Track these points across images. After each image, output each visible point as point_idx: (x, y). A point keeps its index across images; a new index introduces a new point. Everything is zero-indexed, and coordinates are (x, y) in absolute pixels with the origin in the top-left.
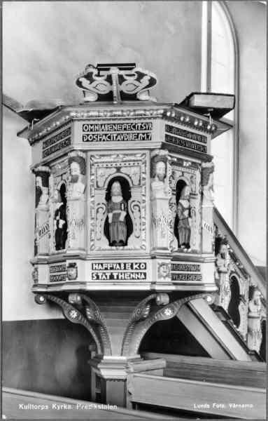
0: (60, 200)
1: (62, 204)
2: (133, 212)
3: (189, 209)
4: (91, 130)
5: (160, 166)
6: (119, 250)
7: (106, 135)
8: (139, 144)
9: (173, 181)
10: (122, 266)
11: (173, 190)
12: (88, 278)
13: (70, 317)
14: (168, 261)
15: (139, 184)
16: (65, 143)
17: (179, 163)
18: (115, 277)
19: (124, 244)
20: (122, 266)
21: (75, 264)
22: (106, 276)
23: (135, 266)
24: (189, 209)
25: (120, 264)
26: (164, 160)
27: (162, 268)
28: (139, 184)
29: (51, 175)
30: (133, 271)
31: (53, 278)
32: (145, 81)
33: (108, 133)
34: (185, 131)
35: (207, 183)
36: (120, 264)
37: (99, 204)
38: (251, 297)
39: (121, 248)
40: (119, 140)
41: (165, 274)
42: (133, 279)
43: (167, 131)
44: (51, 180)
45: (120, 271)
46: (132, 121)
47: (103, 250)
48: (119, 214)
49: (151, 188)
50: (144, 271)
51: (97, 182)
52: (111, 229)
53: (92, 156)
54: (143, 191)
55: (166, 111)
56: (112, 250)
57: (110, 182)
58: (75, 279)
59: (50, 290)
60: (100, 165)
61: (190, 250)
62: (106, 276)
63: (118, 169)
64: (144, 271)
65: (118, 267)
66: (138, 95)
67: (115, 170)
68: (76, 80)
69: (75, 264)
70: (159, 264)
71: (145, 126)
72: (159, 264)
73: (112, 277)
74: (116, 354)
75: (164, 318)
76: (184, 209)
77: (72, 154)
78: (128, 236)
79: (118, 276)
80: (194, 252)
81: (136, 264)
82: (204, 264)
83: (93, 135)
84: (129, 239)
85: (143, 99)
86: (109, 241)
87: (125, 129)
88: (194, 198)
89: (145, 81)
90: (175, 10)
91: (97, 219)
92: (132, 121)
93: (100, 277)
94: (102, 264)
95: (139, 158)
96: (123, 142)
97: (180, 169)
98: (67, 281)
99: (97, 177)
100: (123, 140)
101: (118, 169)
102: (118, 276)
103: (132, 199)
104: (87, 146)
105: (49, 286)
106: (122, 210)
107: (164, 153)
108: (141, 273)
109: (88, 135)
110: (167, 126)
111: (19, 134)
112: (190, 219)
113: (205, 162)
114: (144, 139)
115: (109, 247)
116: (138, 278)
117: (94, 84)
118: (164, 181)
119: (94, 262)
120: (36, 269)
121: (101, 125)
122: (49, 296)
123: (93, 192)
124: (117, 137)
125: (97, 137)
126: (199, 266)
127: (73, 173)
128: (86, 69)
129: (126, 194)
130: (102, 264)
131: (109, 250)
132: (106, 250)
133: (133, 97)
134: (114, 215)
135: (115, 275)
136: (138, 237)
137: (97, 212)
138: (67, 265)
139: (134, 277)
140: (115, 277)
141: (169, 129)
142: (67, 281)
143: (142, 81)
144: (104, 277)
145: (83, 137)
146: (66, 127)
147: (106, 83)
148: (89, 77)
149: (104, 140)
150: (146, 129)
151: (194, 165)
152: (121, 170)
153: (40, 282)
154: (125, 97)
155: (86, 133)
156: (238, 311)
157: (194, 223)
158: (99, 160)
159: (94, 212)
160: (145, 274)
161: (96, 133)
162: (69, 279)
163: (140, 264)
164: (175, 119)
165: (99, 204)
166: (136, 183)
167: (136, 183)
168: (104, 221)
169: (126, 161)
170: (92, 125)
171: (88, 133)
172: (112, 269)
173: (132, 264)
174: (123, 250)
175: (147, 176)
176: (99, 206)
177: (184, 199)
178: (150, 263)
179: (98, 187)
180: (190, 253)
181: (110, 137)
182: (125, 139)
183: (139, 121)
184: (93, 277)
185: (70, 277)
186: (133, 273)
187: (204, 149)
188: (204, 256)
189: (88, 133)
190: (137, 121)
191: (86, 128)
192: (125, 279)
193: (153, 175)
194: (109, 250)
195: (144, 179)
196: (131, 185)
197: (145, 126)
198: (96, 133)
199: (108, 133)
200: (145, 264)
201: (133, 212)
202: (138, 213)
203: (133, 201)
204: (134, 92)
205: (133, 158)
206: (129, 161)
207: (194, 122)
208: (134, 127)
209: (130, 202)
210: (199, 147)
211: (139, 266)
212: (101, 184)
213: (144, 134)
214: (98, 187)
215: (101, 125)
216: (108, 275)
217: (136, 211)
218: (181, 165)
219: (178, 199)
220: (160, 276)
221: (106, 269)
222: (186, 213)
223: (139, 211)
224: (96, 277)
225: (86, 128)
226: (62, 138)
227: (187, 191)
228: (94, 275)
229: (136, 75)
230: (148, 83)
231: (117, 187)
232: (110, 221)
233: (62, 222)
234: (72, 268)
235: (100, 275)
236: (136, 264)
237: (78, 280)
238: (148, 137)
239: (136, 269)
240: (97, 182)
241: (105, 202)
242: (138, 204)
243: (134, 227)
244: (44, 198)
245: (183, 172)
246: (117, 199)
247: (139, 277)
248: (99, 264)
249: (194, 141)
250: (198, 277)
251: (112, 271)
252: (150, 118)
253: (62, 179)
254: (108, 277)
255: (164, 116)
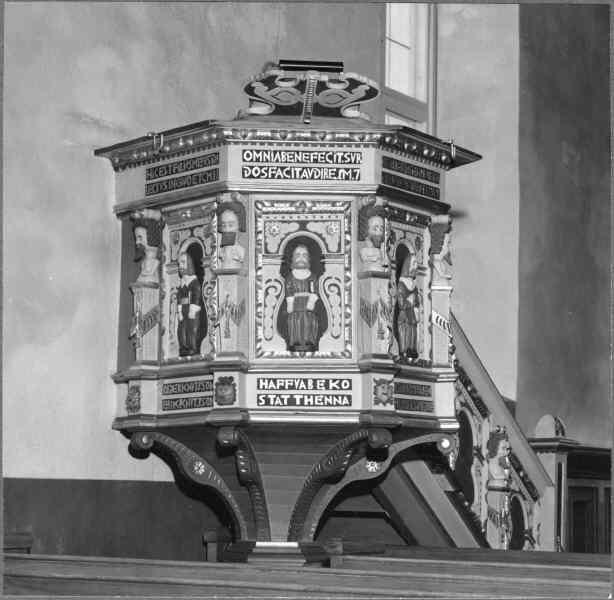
0: (192, 270)
1: (194, 277)
2: (328, 296)
3: (415, 291)
4: (258, 160)
5: (376, 223)
6: (307, 358)
7: (282, 168)
8: (338, 184)
9: (392, 246)
10: (310, 383)
11: (393, 262)
12: (251, 403)
13: (193, 474)
14: (389, 377)
15: (339, 250)
16: (205, 177)
17: (399, 217)
18: (298, 402)
19: (314, 348)
20: (310, 383)
21: (231, 378)
22: (282, 400)
23: (332, 385)
24: (415, 291)
25: (306, 381)
26: (382, 214)
27: (380, 388)
28: (339, 250)
29: (167, 226)
30: (328, 392)
31: (167, 405)
32: (360, 91)
33: (286, 165)
34: (408, 165)
35: (441, 249)
36: (306, 381)
37: (269, 281)
38: (493, 452)
39: (308, 354)
40: (305, 178)
41: (385, 398)
42: (329, 404)
43: (384, 166)
44: (167, 235)
45: (307, 392)
46: (327, 148)
47: (278, 357)
48: (307, 298)
49: (360, 255)
50: (348, 393)
51: (266, 244)
52: (291, 322)
53: (257, 202)
54: (347, 261)
55: (384, 136)
56: (187, 361)
57: (290, 242)
58: (232, 404)
59: (163, 423)
60: (272, 217)
61: (417, 360)
62: (282, 400)
63: (303, 225)
64: (348, 393)
65: (303, 385)
66: (342, 109)
67: (297, 226)
68: (248, 83)
69: (231, 378)
70: (375, 380)
71: (349, 156)
72: (375, 380)
73: (292, 401)
74: (279, 538)
75: (376, 464)
76: (408, 293)
77: (226, 198)
78: (320, 335)
79: (302, 400)
80: (423, 363)
81: (334, 381)
82: (436, 384)
83: (261, 168)
84: (322, 339)
85: (347, 115)
86: (288, 342)
87: (316, 161)
88: (420, 274)
89: (360, 91)
90: (423, 8)
91: (265, 306)
92: (327, 148)
93: (272, 403)
94: (275, 381)
95: (338, 209)
96: (311, 182)
97: (401, 226)
98: (216, 406)
99: (265, 237)
100: (312, 178)
101: (303, 225)
102: (302, 400)
103: (326, 275)
104: (250, 185)
105: (159, 417)
106: (310, 291)
107: (380, 201)
108: (343, 396)
109: (252, 167)
110: (384, 158)
111: (98, 152)
112: (416, 309)
113: (437, 214)
114: (347, 178)
115: (289, 353)
116: (338, 405)
117: (275, 91)
118: (379, 248)
119: (260, 376)
120: (137, 389)
121: (275, 152)
122: (157, 435)
123: (260, 260)
124: (301, 173)
125: (267, 171)
126: (429, 387)
127: (228, 229)
128: (264, 71)
129: (317, 265)
130: (275, 381)
131: (287, 357)
132: (282, 357)
133: (336, 113)
134: (297, 300)
135: (298, 398)
136: (271, 339)
137: (267, 293)
138: (216, 381)
139: (330, 401)
140: (298, 402)
141: (387, 162)
142: (216, 406)
143: (353, 91)
144: (278, 401)
145: (243, 169)
146: (212, 150)
147: (294, 90)
148: (270, 82)
149: (279, 177)
150: (350, 162)
151: (422, 222)
152: (308, 226)
153: (143, 411)
154: (321, 111)
155: (248, 164)
156: (470, 476)
157: (423, 313)
158: (270, 209)
159: (261, 293)
160: (349, 397)
161: (266, 164)
162: (219, 404)
163: (341, 380)
164: (397, 147)
165: (269, 281)
166: (333, 248)
167: (333, 248)
168: (278, 308)
169: (317, 212)
170: (258, 152)
171: (251, 164)
172: (292, 388)
173: (327, 381)
174: (312, 357)
175: (353, 238)
176: (269, 284)
177: (407, 277)
178: (357, 379)
179: (267, 251)
180: (416, 365)
181: (289, 172)
182: (316, 177)
183: (340, 149)
184: (259, 401)
185: (221, 400)
186: (328, 396)
187: (436, 193)
188: (434, 370)
189: (251, 164)
190: (336, 149)
191: (248, 156)
192: (314, 405)
193: (362, 236)
194: (287, 357)
195: (348, 242)
196: (325, 252)
197: (349, 156)
198: (266, 164)
199: (286, 165)
200: (350, 381)
201: (328, 296)
202: (337, 297)
203: (329, 278)
204: (335, 106)
205: (328, 207)
206: (321, 212)
207: (423, 150)
208: (331, 157)
209: (322, 278)
210: (428, 190)
211: (339, 385)
212: (272, 248)
213: (347, 170)
214: (267, 251)
215: (275, 152)
216: (286, 398)
217: (334, 298)
218: (402, 220)
219: (398, 275)
220: (377, 402)
221: (282, 388)
222: (411, 299)
223: (339, 294)
224: (263, 402)
225: (248, 156)
226: (196, 168)
227: (412, 263)
228: (261, 398)
229: (347, 82)
230: (363, 94)
231: (301, 253)
232: (290, 309)
233: (194, 309)
234: (226, 387)
235: (272, 397)
236: (334, 381)
237: (236, 404)
238: (354, 174)
239: (334, 389)
240: (266, 244)
241: (278, 276)
242: (337, 282)
243: (330, 320)
244: (150, 264)
245: (405, 232)
246: (301, 274)
247: (340, 402)
248: (269, 380)
249: (422, 181)
250: (429, 406)
251: (292, 392)
252: (358, 146)
253: (192, 235)
254: (286, 402)
255: (381, 143)
